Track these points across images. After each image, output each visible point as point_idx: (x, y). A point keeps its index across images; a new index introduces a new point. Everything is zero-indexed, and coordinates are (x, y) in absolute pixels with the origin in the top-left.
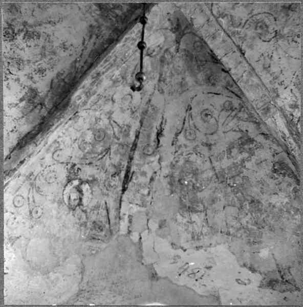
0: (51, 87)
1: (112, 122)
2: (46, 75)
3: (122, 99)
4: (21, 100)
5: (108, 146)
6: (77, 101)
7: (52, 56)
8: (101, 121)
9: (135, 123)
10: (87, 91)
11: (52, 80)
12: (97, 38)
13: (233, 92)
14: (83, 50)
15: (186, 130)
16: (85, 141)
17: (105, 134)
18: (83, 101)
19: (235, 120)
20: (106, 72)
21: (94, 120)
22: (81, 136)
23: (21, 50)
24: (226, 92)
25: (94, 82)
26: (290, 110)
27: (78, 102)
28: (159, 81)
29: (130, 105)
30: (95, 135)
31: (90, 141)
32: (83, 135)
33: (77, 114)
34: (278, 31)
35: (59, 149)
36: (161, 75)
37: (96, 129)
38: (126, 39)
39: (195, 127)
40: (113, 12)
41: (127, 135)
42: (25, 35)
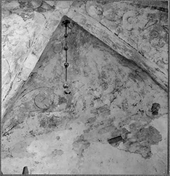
0: (127, 66)
1: (145, 28)
2: (121, 69)
4: (135, 81)
5: (161, 28)
6: (130, 56)
7: (112, 65)
8: (145, 35)
9: (146, 11)
10: (123, 51)
11: (123, 66)
12: (98, 44)
14: (106, 51)
16: (158, 44)
17: (153, 31)
18: (130, 52)
20: (112, 42)
21: (144, 40)
23: (111, 80)
27: (130, 55)
29: (134, 17)
30: (154, 38)
32: (154, 46)
33: (140, 52)
35: (162, 60)
38: (93, 33)
40: (84, 37)
42: (104, 78)
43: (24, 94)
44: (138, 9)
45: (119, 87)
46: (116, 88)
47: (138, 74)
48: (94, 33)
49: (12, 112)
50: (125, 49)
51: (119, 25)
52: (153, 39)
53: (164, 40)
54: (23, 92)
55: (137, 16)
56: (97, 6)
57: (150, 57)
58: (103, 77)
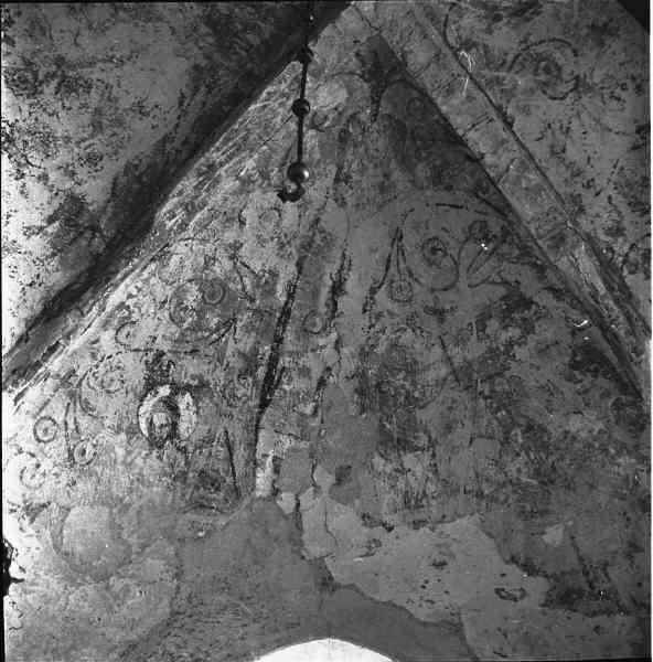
0: (113, 194)
1: (239, 264)
2: (102, 168)
4: (51, 220)
6: (167, 222)
11: (115, 179)
13: (488, 203)
14: (179, 118)
15: (392, 282)
19: (493, 262)
24: (474, 203)
26: (609, 239)
27: (169, 224)
28: (337, 180)
31: (194, 305)
34: (582, 76)
36: (340, 168)
39: (411, 275)
41: (272, 292)
42: (59, 84)
44: (298, 242)
45: (21, 146)
46: (16, 135)
47: (81, 234)
48: (268, 100)
50: (193, 204)
51: (266, 182)
52: (200, 290)
53: (191, 324)
55: (279, 238)
56: (340, 114)
57: (146, 281)
58: (64, 78)
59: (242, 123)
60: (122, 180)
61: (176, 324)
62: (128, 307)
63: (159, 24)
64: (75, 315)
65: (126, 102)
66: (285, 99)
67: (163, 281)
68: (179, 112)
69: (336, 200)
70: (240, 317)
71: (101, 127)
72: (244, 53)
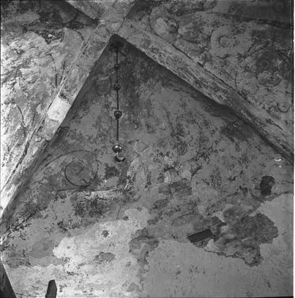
1: (248, 53)
3: (224, 47)
4: (233, 140)
6: (223, 99)
10: (213, 91)
17: (262, 58)
20: (193, 76)
22: (264, 85)
25: (204, 85)
27: (224, 98)
28: (203, 10)
31: (270, 73)
36: (197, 10)
37: (257, 69)
41: (263, 32)
43: (47, 163)
45: (205, 151)
49: (28, 191)
51: (206, 49)
52: (262, 72)
54: (46, 159)
57: (256, 101)
59: (176, 72)
60: (212, 113)
61: (279, 82)
62: (269, 108)
63: (151, 99)
64: (269, 137)
65: (182, 111)
66: (162, 55)
67: (257, 93)
68: (181, 91)
69: (213, 7)
70: (277, 48)
71: (194, 120)
72: (152, 67)
